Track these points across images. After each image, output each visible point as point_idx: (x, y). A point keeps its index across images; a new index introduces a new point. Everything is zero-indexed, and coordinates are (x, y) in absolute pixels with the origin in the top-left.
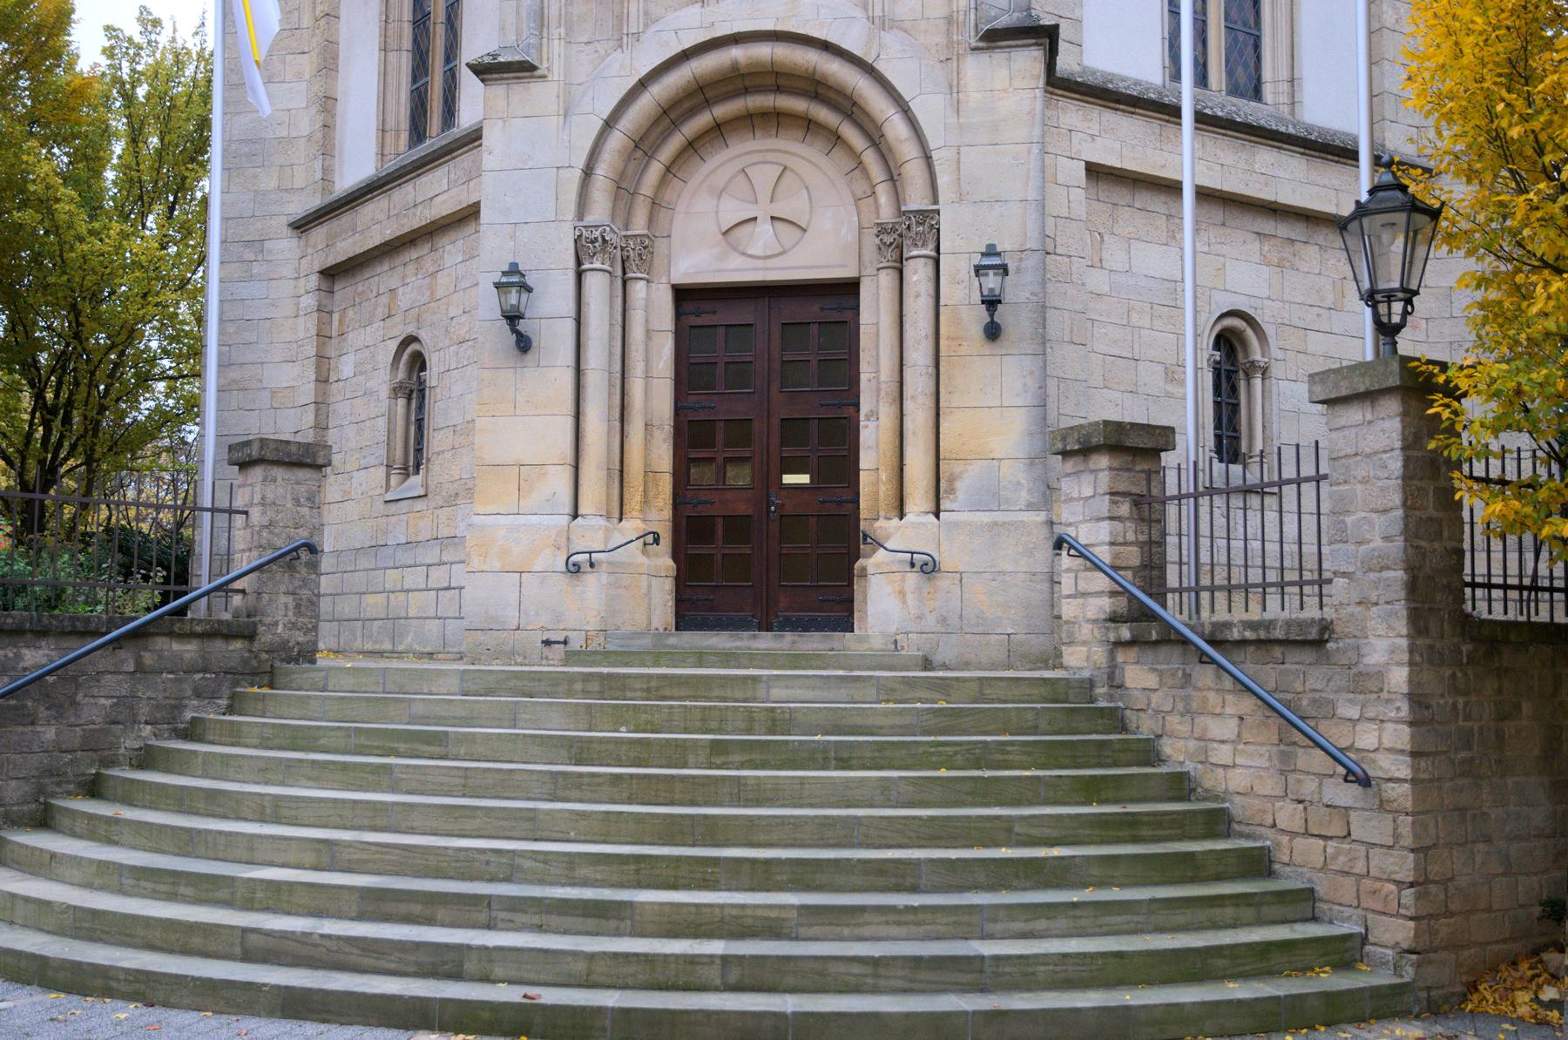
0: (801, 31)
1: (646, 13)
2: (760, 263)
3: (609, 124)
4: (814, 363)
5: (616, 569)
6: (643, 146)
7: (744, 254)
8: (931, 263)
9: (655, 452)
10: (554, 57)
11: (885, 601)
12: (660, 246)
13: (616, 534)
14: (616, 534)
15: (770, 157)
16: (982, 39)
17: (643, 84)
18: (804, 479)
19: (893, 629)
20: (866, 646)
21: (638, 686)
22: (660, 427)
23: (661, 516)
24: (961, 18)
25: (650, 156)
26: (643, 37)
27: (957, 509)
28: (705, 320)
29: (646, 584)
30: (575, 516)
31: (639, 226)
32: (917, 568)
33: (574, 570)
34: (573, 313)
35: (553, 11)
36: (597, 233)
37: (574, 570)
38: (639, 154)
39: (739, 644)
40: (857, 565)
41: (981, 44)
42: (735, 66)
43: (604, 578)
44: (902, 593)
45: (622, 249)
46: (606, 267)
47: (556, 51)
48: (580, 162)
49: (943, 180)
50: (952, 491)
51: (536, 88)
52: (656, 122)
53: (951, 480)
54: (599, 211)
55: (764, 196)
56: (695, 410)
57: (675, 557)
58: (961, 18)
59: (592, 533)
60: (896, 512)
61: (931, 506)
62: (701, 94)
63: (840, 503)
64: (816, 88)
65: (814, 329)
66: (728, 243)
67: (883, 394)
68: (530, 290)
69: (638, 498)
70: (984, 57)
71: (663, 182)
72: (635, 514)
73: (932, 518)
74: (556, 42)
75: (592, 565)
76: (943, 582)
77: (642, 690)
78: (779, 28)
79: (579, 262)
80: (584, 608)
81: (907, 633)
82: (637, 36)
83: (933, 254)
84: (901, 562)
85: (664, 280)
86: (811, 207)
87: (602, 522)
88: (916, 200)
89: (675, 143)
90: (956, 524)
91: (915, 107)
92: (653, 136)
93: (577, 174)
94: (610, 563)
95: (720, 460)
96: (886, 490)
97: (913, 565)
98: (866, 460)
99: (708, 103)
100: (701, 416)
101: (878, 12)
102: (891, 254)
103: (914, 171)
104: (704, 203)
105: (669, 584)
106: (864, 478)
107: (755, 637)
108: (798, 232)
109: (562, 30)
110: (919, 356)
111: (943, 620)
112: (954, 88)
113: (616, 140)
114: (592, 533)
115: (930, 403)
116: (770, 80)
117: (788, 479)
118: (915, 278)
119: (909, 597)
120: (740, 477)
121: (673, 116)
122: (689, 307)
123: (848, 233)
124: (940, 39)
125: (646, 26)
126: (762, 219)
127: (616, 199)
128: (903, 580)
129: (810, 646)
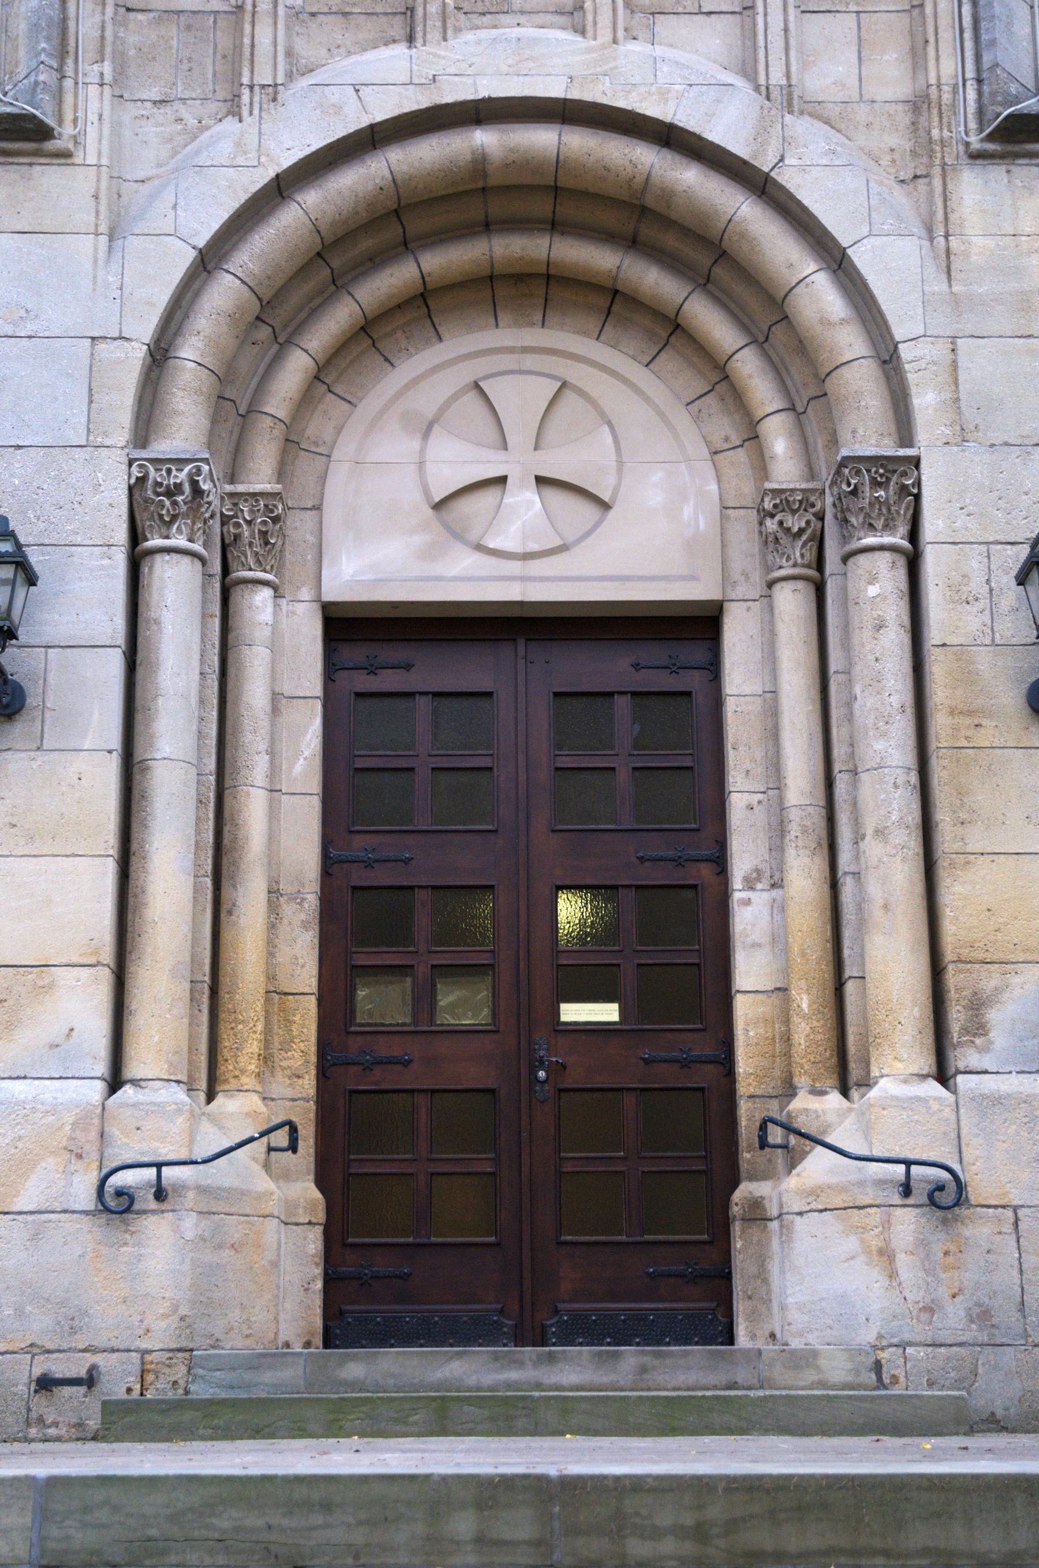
0: (621, 103)
1: (289, 53)
2: (515, 567)
3: (209, 261)
4: (623, 776)
5: (214, 1202)
6: (275, 316)
7: (480, 548)
8: (901, 562)
9: (282, 948)
10: (88, 114)
11: (825, 1271)
12: (299, 527)
13: (206, 1127)
14: (206, 1127)
15: (530, 361)
16: (991, 138)
17: (281, 188)
18: (607, 1012)
19: (868, 1336)
20: (810, 1376)
21: (665, 1519)
22: (296, 897)
23: (297, 1090)
24: (946, 97)
25: (284, 341)
26: (283, 95)
27: (990, 1071)
28: (388, 681)
29: (243, 1239)
30: (115, 1082)
31: (260, 479)
32: (919, 1196)
33: (116, 1206)
34: (120, 638)
35: (87, 24)
36: (182, 476)
37: (116, 1206)
38: (264, 333)
39: (513, 1375)
40: (738, 1195)
41: (991, 147)
42: (480, 164)
43: (190, 1225)
44: (886, 1255)
45: (225, 520)
46: (197, 547)
47: (94, 106)
48: (144, 328)
49: (925, 401)
50: (978, 1028)
51: (48, 177)
52: (303, 271)
53: (977, 1005)
54: (184, 432)
55: (519, 435)
56: (369, 865)
57: (321, 1182)
58: (946, 97)
59: (160, 1118)
60: (832, 1080)
61: (926, 1062)
62: (398, 222)
63: (685, 1064)
64: (641, 220)
65: (623, 704)
66: (446, 526)
67: (794, 829)
68: (32, 580)
69: (253, 1047)
70: (997, 173)
71: (306, 401)
72: (248, 1082)
73: (934, 1088)
74: (93, 90)
75: (160, 1194)
76: (979, 1230)
77: (680, 1532)
78: (574, 94)
79: (135, 536)
80: (145, 1293)
81: (903, 1345)
82: (273, 92)
83: (905, 544)
84: (881, 1183)
85: (306, 593)
86: (620, 463)
87: (180, 1094)
88: (867, 435)
89: (338, 319)
90: (997, 1100)
91: (861, 257)
92: (295, 298)
93: (137, 354)
94: (203, 1190)
95: (422, 971)
96: (808, 1031)
97: (907, 1190)
98: (750, 971)
99: (406, 246)
100: (382, 877)
101: (777, 77)
102: (799, 552)
103: (860, 382)
104: (395, 446)
105: (314, 1242)
106: (743, 1008)
107: (551, 1358)
108: (587, 511)
109: (107, 68)
110: (888, 748)
111: (982, 1315)
112: (938, 228)
113: (224, 293)
114: (160, 1118)
115: (914, 845)
116: (541, 207)
117: (572, 1012)
118: (873, 591)
119: (904, 1262)
120: (463, 1006)
121: (336, 263)
122: (353, 653)
123: (697, 516)
124: (898, 140)
125: (290, 76)
126: (521, 481)
127: (215, 420)
128: (887, 1224)
129: (681, 1378)
